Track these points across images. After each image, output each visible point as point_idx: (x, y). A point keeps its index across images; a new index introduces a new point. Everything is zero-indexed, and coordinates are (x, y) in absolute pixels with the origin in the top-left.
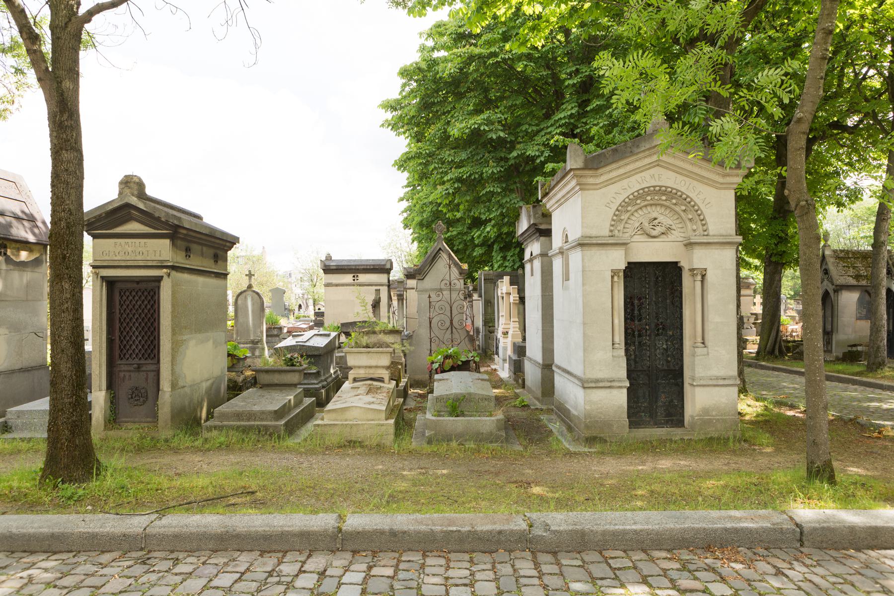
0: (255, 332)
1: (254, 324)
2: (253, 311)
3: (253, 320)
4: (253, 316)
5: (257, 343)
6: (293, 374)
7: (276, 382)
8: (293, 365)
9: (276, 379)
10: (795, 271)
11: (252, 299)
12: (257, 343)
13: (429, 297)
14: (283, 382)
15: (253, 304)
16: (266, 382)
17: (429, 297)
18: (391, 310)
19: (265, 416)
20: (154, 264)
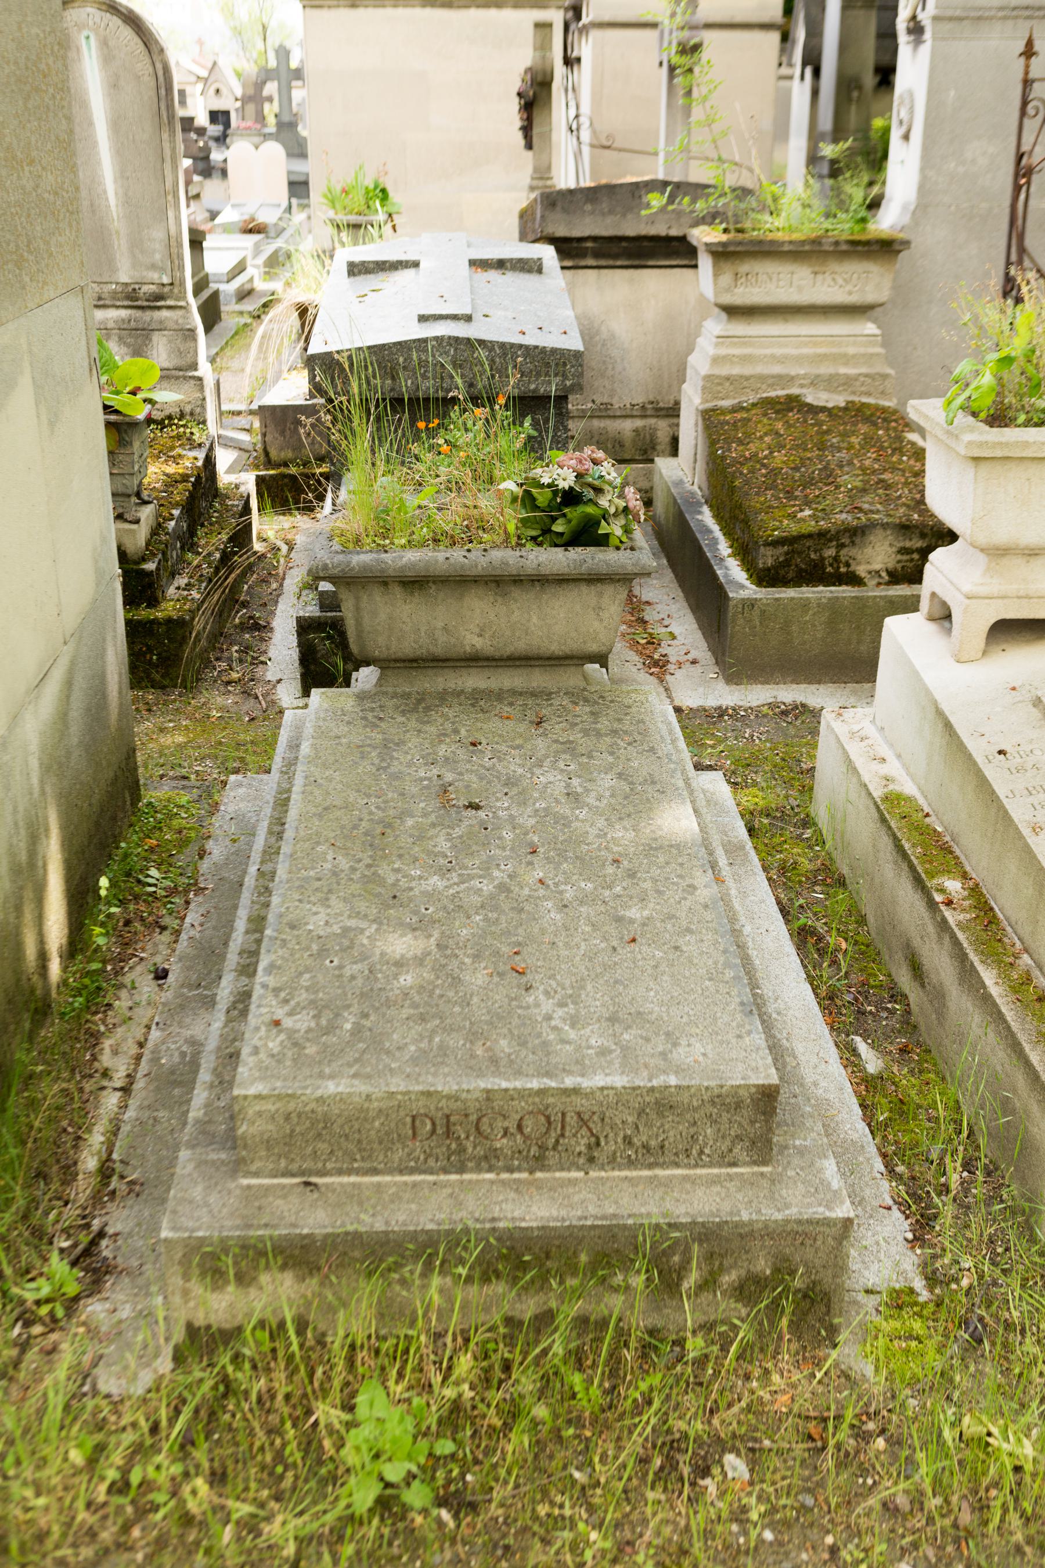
0: (137, 244)
1: (127, 200)
2: (116, 125)
3: (122, 175)
4: (119, 151)
5: (156, 300)
6: (588, 594)
7: (473, 641)
8: (587, 535)
9: (476, 623)
10: (80, 27)
11: (107, 57)
12: (156, 300)
13: (1029, 52)
14: (520, 646)
15: (114, 86)
16: (407, 647)
17: (1029, 52)
18: (904, 129)
19: (674, 1131)
20: (473, 680)
